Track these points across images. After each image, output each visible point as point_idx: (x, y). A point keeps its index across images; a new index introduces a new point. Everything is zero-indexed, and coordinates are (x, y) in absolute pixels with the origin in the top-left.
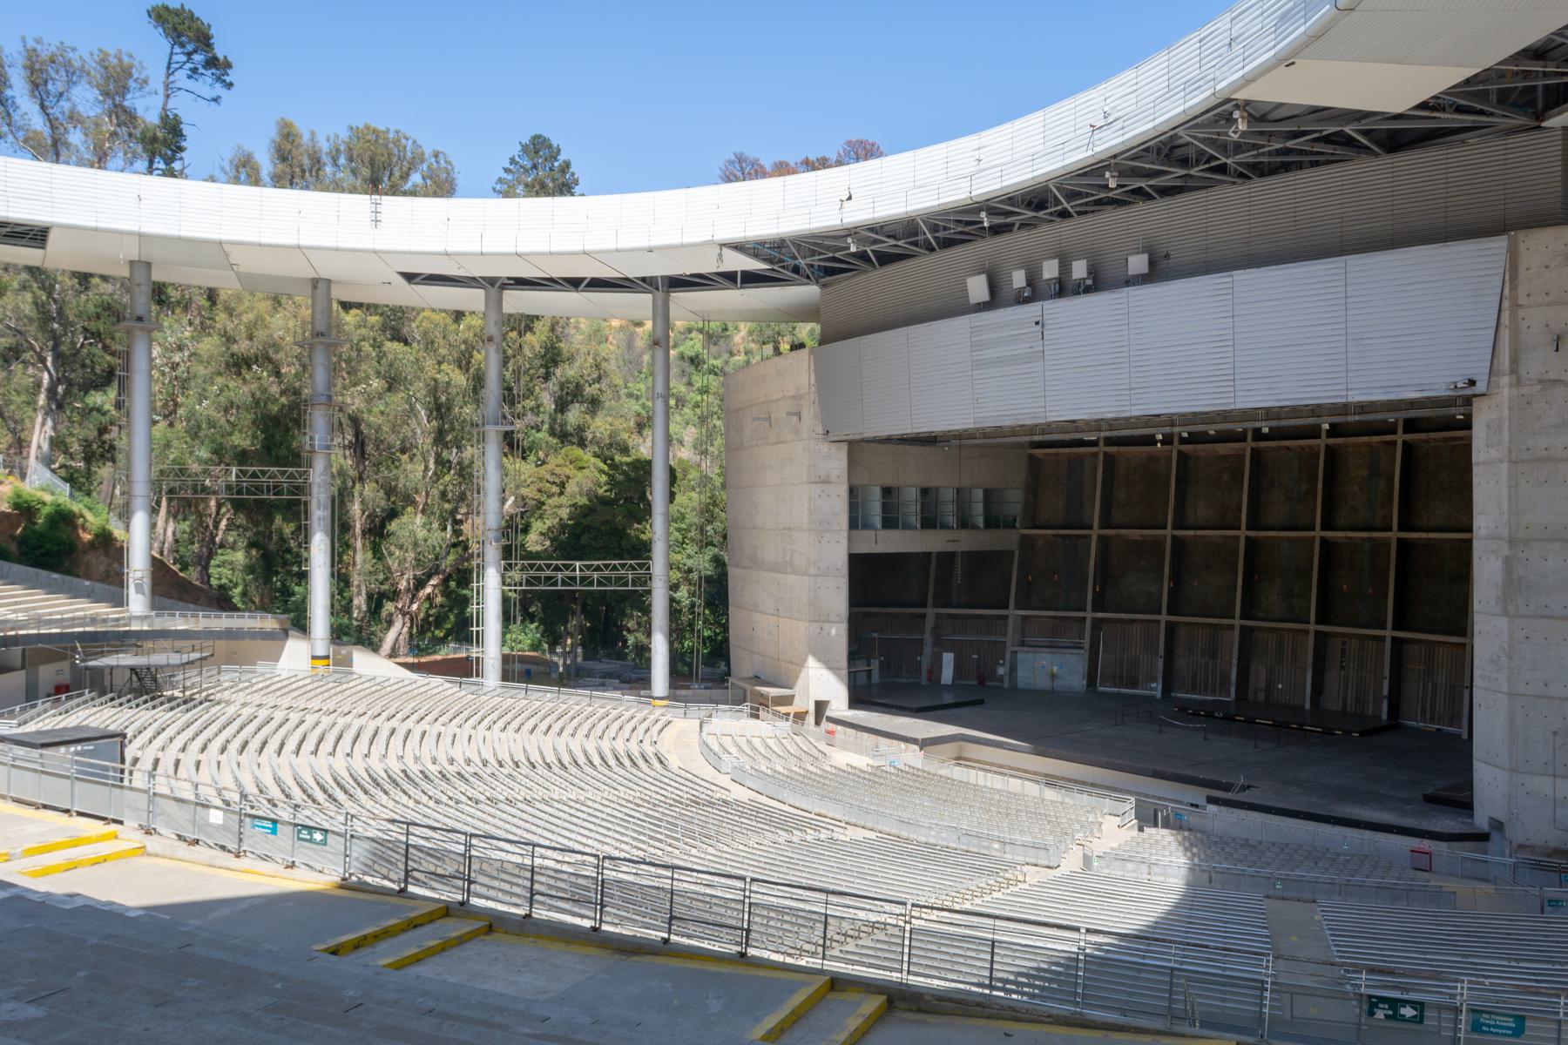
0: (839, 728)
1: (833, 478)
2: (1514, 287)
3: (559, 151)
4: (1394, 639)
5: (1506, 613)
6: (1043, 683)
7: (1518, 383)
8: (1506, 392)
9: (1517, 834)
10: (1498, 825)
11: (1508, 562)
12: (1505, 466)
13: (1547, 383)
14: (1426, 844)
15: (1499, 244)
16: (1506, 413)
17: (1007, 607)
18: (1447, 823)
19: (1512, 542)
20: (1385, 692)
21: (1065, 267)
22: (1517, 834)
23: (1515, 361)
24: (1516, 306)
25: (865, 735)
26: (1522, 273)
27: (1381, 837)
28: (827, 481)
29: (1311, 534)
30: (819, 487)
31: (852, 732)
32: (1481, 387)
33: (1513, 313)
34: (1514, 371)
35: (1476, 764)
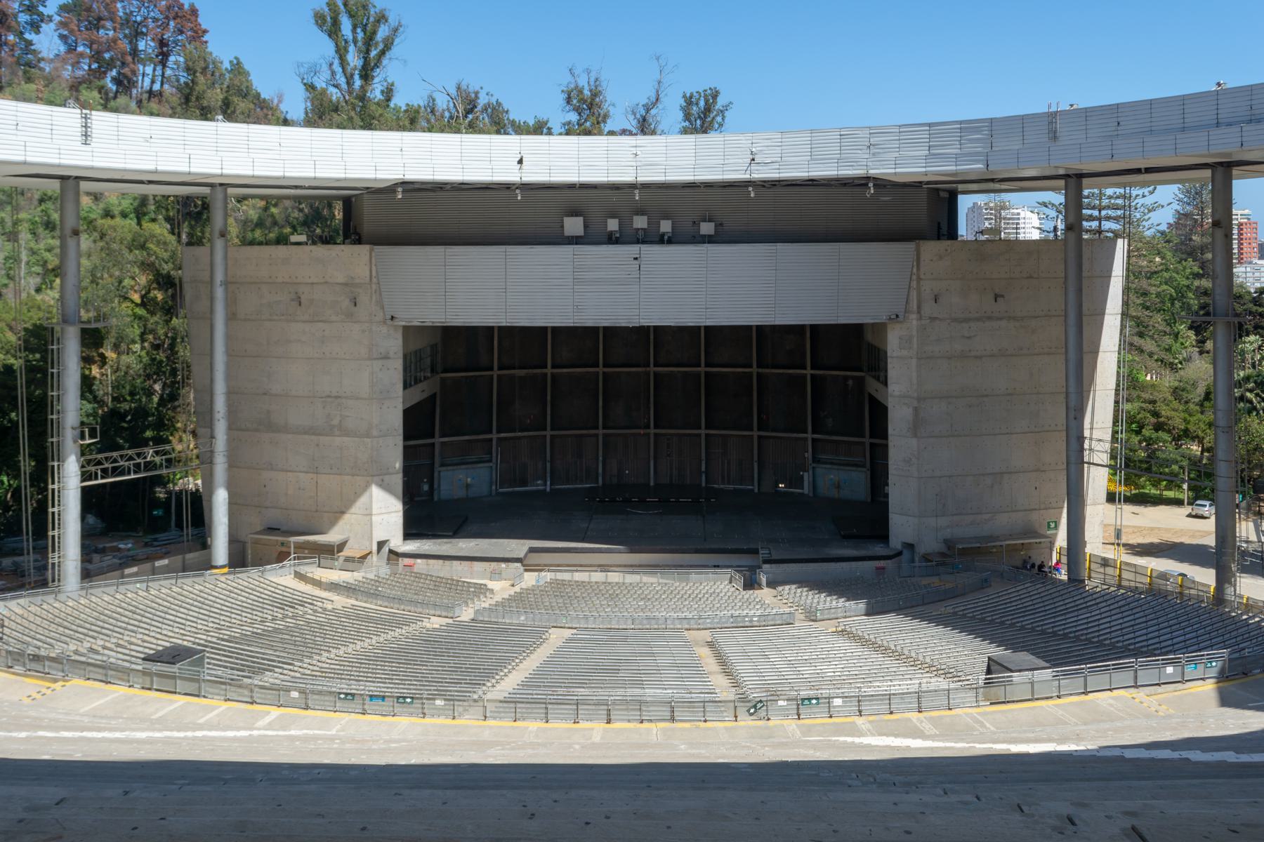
0: (419, 561)
1: (391, 354)
2: (918, 269)
3: (606, 116)
4: (656, 435)
5: (915, 436)
6: (460, 493)
7: (920, 318)
8: (915, 322)
9: (922, 549)
10: (910, 546)
11: (916, 409)
12: (914, 361)
13: (933, 319)
14: (882, 563)
15: (910, 246)
16: (915, 333)
17: (433, 437)
18: (879, 549)
19: (919, 399)
20: (703, 469)
21: (654, 223)
22: (922, 549)
23: (919, 307)
24: (919, 279)
25: (455, 563)
26: (922, 263)
27: (854, 564)
28: (386, 358)
29: (544, 371)
30: (380, 362)
31: (441, 562)
32: (901, 318)
33: (918, 283)
34: (919, 312)
35: (891, 516)
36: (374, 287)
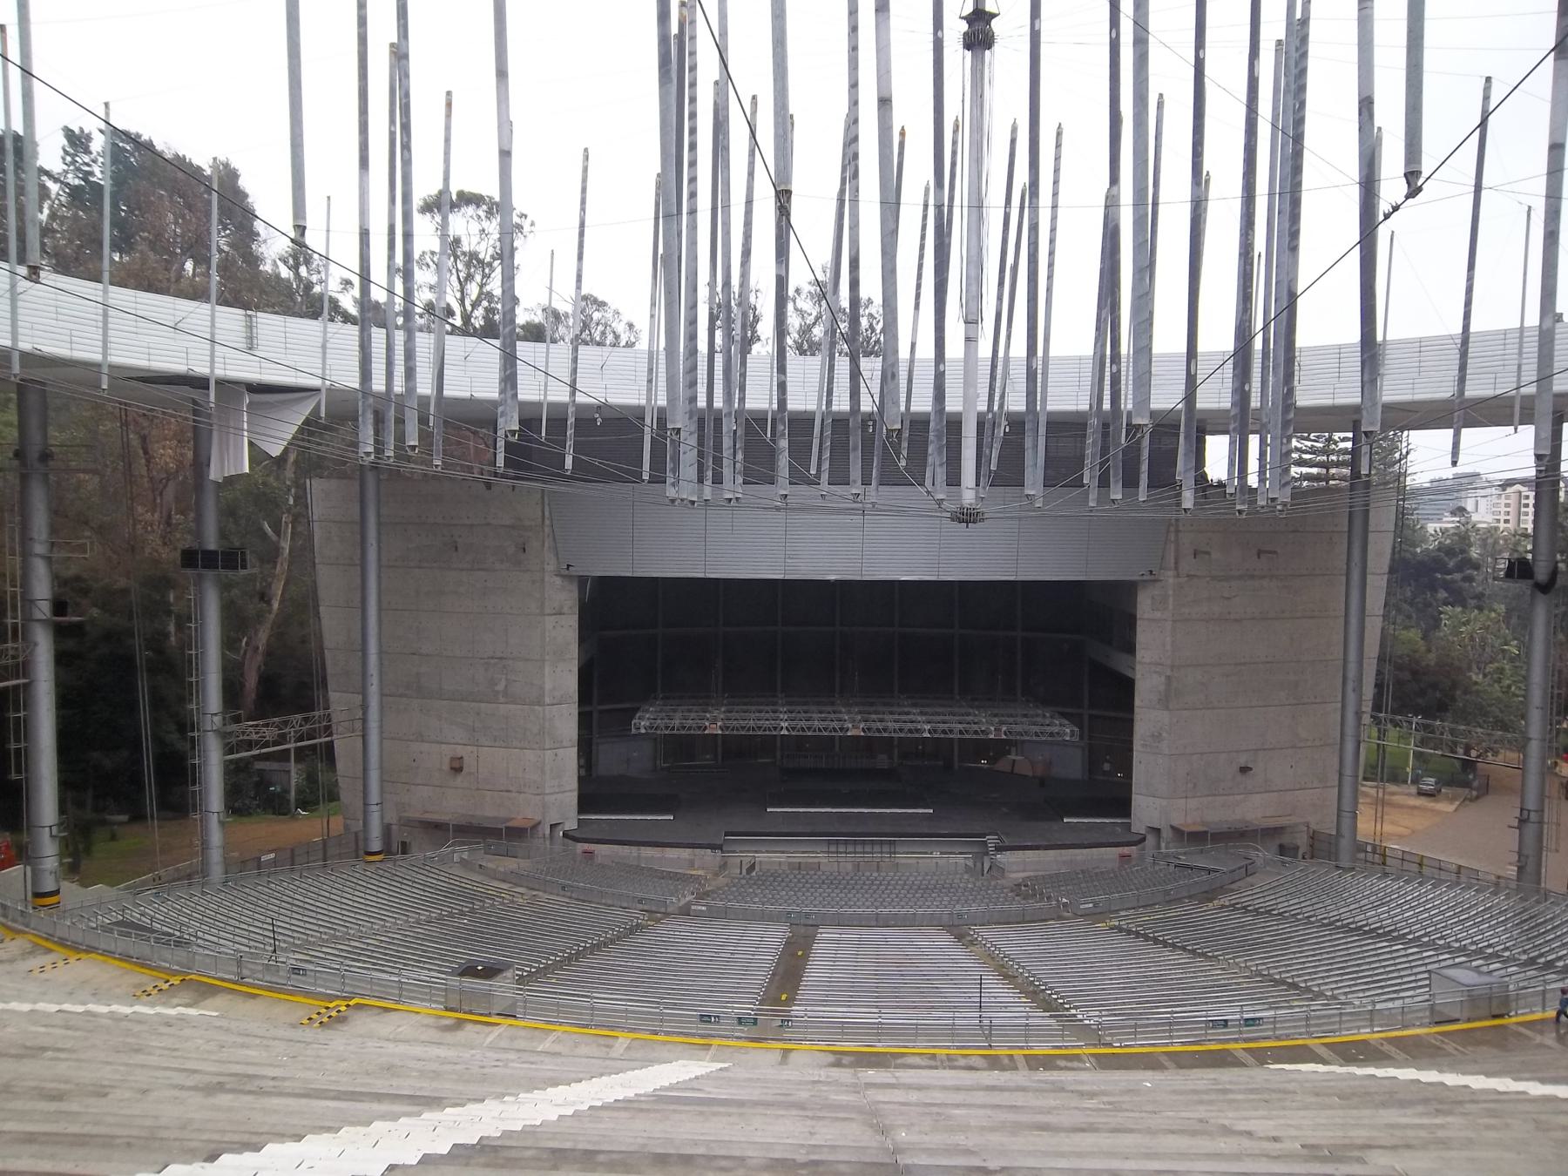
1: (565, 610)
8: (1171, 580)
23: (1176, 563)
34: (1176, 568)
36: (547, 530)
